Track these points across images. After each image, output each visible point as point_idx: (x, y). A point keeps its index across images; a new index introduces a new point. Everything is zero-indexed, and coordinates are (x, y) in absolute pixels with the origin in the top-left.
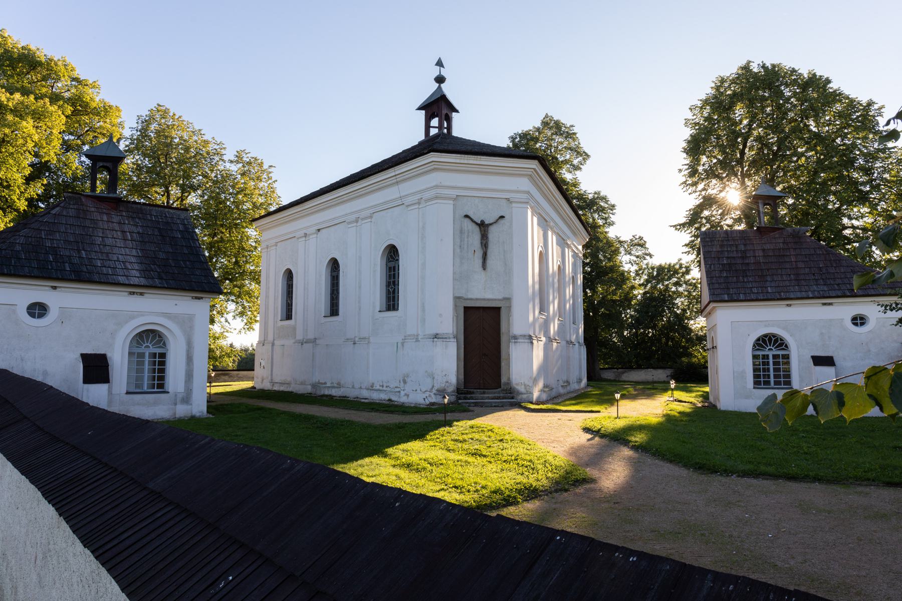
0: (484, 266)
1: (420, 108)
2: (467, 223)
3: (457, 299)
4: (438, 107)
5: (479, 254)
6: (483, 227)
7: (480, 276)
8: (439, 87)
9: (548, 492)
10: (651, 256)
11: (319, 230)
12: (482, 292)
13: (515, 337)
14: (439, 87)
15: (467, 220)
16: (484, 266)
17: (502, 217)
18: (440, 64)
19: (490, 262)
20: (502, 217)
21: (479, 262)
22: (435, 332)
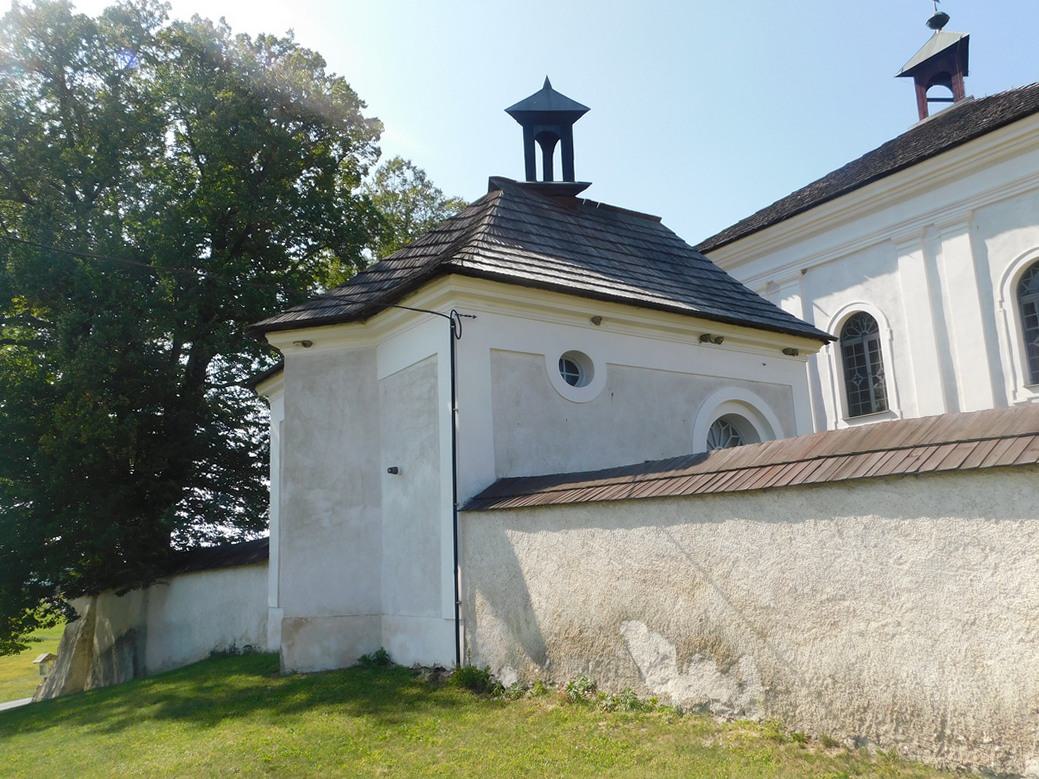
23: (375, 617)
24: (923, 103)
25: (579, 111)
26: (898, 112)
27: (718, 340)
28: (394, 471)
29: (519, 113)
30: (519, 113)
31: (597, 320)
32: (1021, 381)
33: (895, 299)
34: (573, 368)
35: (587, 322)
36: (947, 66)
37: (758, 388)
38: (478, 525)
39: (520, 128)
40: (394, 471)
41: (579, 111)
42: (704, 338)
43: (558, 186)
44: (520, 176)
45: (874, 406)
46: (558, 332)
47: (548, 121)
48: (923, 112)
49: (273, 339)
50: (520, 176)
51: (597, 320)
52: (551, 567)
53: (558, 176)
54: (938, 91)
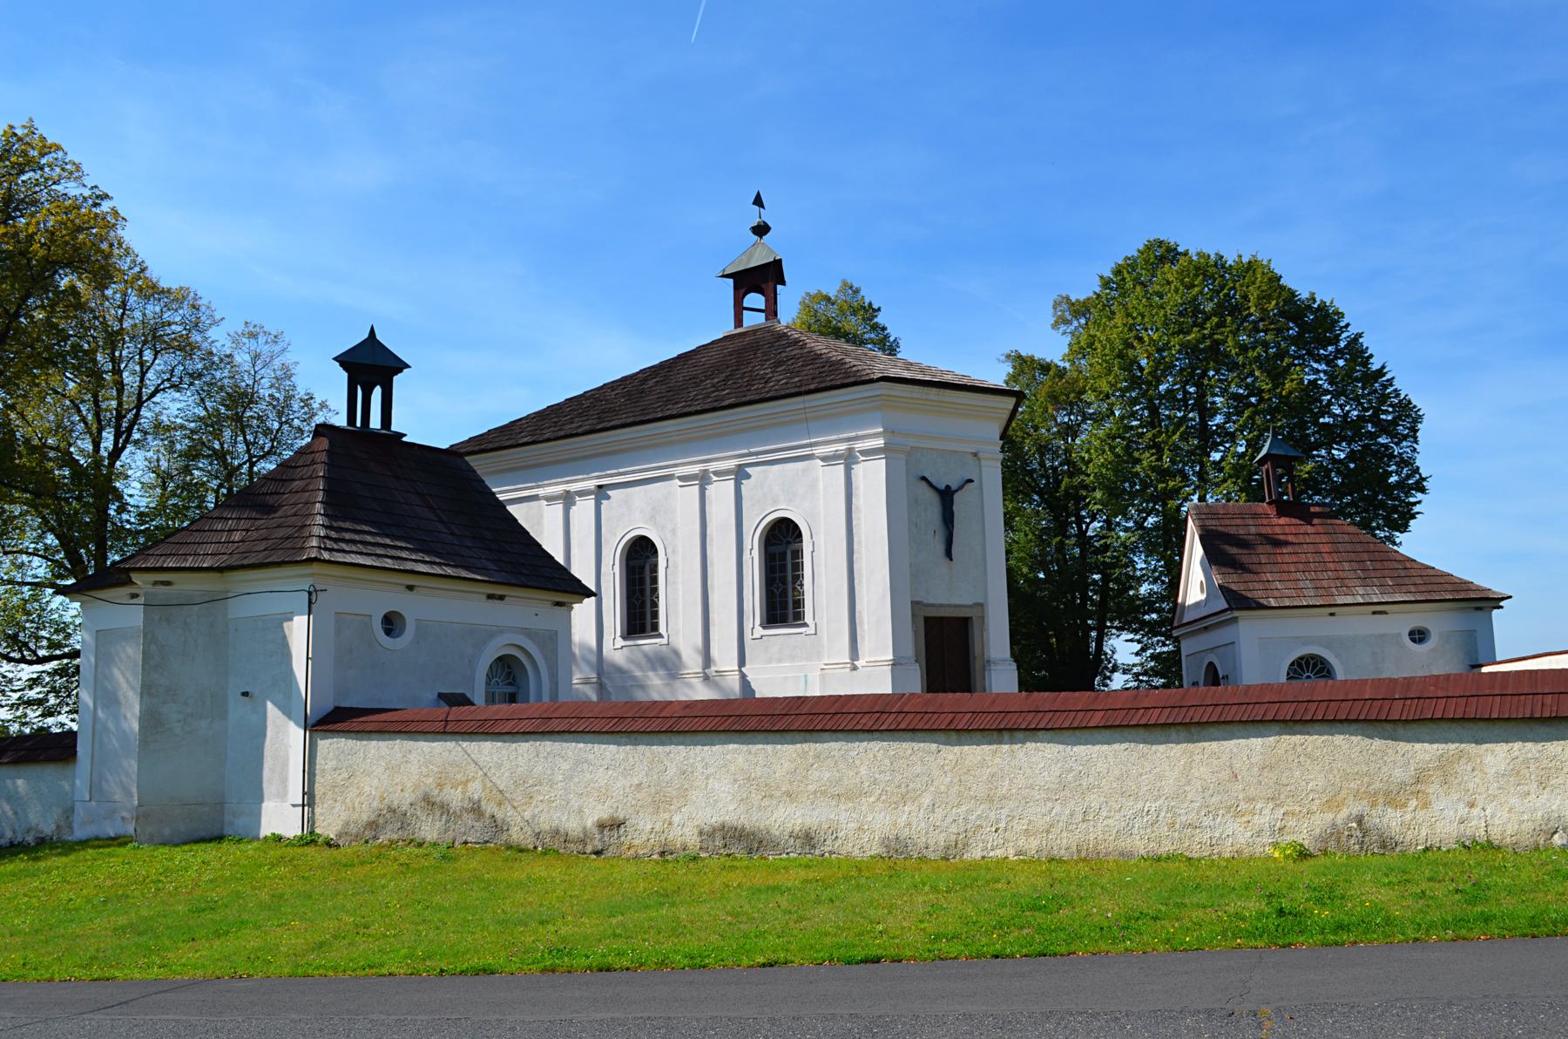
0: (949, 554)
3: (915, 604)
6: (946, 496)
10: (106, 197)
12: (949, 595)
15: (923, 484)
16: (949, 554)
17: (971, 481)
18: (758, 201)
20: (971, 481)
21: (941, 548)
23: (220, 805)
24: (739, 309)
25: (400, 366)
26: (708, 320)
27: (501, 598)
28: (245, 694)
29: (344, 360)
30: (344, 360)
31: (410, 588)
32: (758, 621)
33: (674, 531)
34: (392, 623)
35: (403, 589)
36: (760, 279)
37: (529, 633)
38: (329, 747)
39: (345, 375)
40: (245, 694)
41: (400, 366)
42: (490, 597)
43: (374, 433)
44: (341, 421)
45: (649, 627)
46: (378, 598)
47: (371, 367)
48: (739, 321)
49: (135, 577)
50: (341, 421)
51: (410, 588)
52: (380, 770)
53: (375, 422)
54: (755, 300)
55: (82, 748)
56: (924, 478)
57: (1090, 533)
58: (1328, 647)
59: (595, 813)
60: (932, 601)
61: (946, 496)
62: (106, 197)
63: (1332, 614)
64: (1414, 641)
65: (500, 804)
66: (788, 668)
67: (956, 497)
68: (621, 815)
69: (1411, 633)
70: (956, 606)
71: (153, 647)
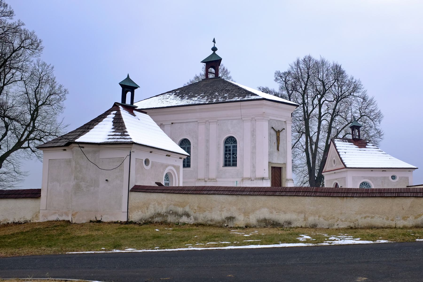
0: (278, 149)
1: (203, 62)
2: (272, 130)
3: (269, 163)
4: (213, 63)
5: (276, 145)
6: (278, 133)
7: (334, 165)
8: (214, 53)
9: (402, 228)
10: (23, 24)
11: (172, 123)
12: (277, 161)
13: (287, 180)
14: (214, 53)
15: (272, 129)
16: (278, 149)
17: (284, 129)
18: (214, 41)
19: (280, 148)
20: (284, 129)
21: (276, 147)
22: (262, 177)
25: (136, 87)
27: (169, 156)
28: (107, 180)
29: (120, 84)
38: (134, 195)
40: (107, 180)
55: (43, 194)
56: (272, 128)
57: (35, 108)
58: (370, 180)
59: (225, 214)
60: (273, 162)
61: (278, 133)
62: (23, 24)
63: (372, 171)
64: (392, 179)
65: (195, 213)
66: (230, 178)
67: (281, 133)
68: (234, 216)
69: (392, 177)
70: (279, 164)
71: (78, 165)
